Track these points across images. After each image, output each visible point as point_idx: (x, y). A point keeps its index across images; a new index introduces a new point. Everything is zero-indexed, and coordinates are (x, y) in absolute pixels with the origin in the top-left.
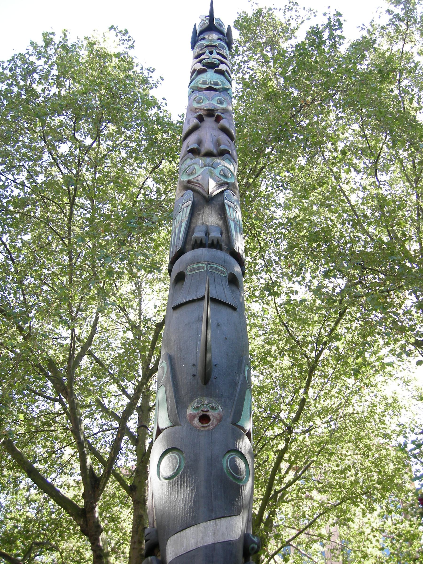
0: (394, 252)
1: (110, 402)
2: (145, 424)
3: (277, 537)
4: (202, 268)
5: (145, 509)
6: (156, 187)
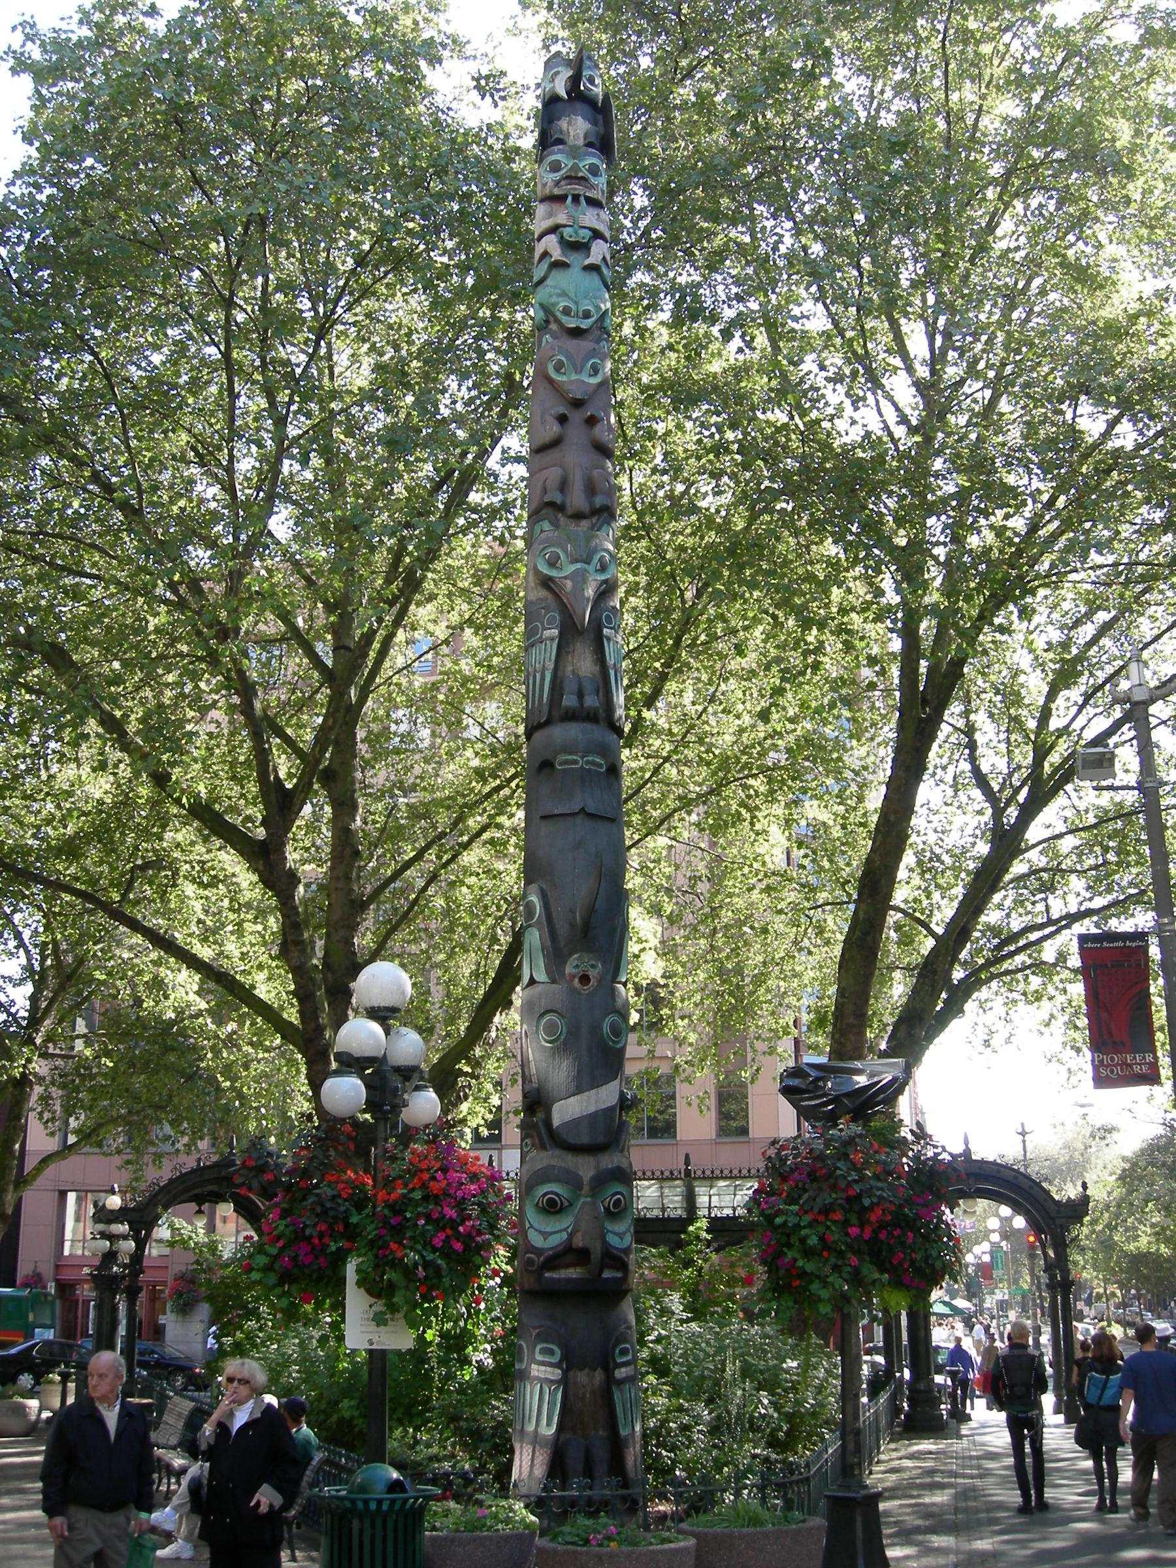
4: (576, 762)
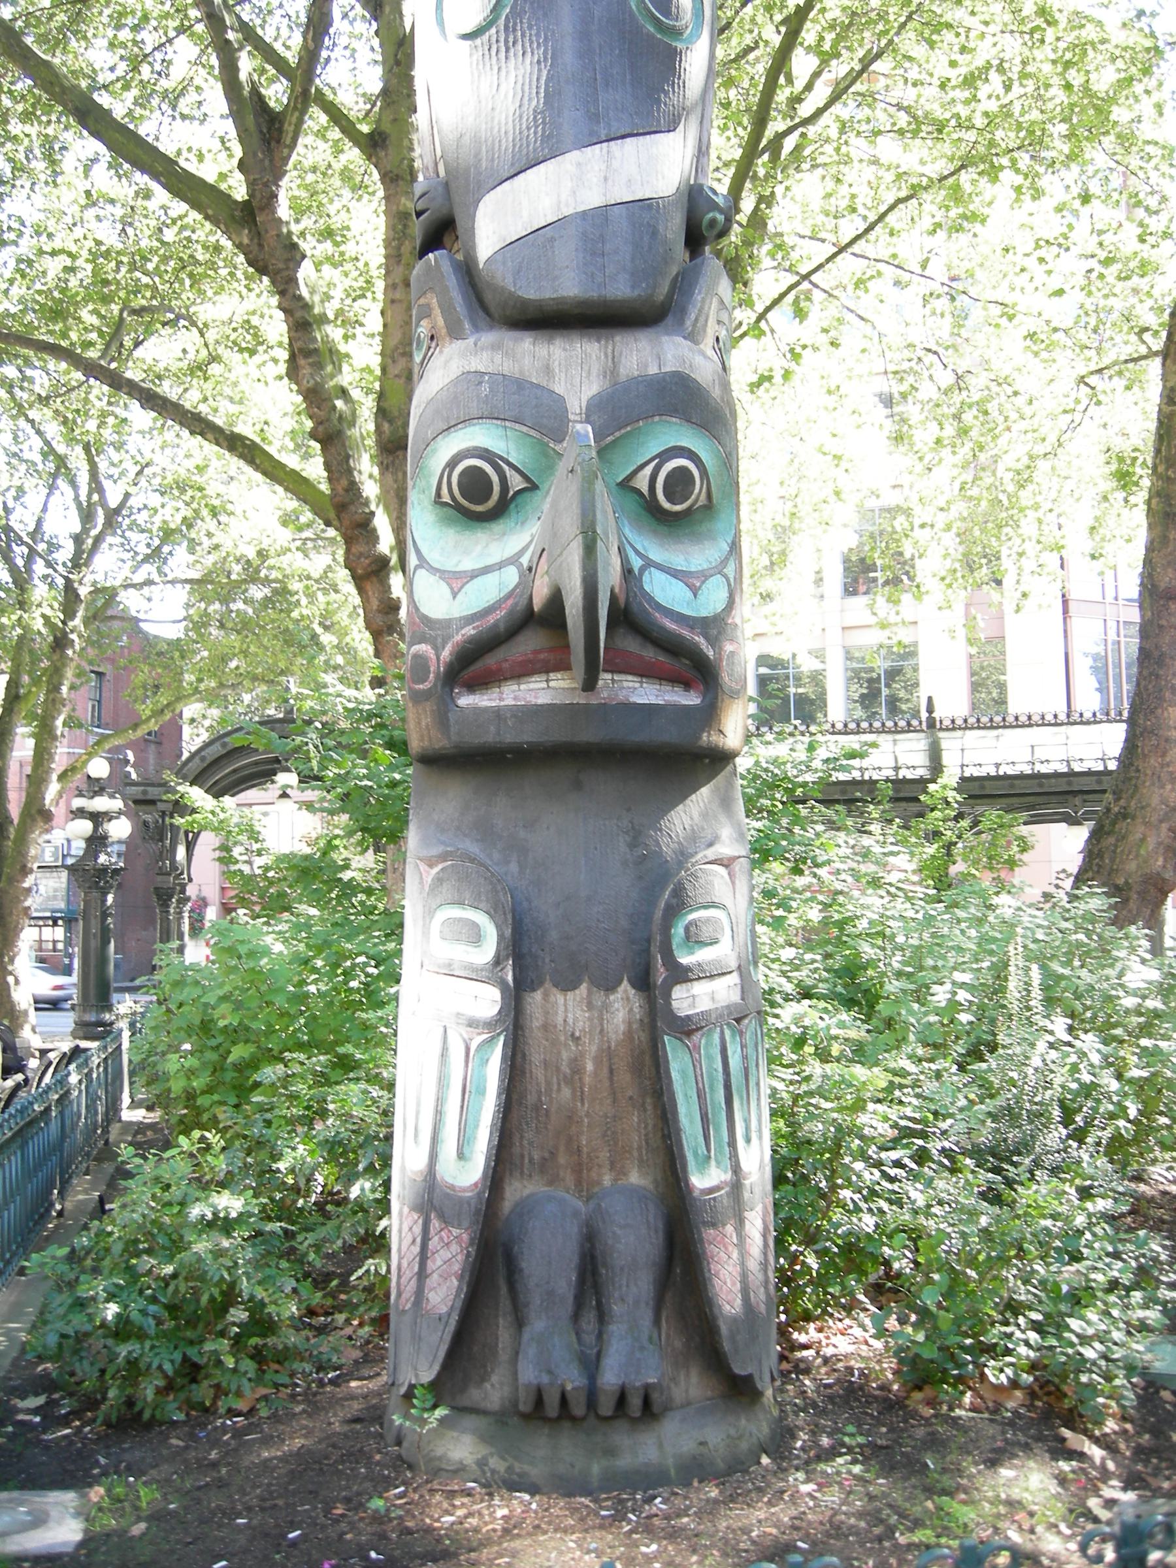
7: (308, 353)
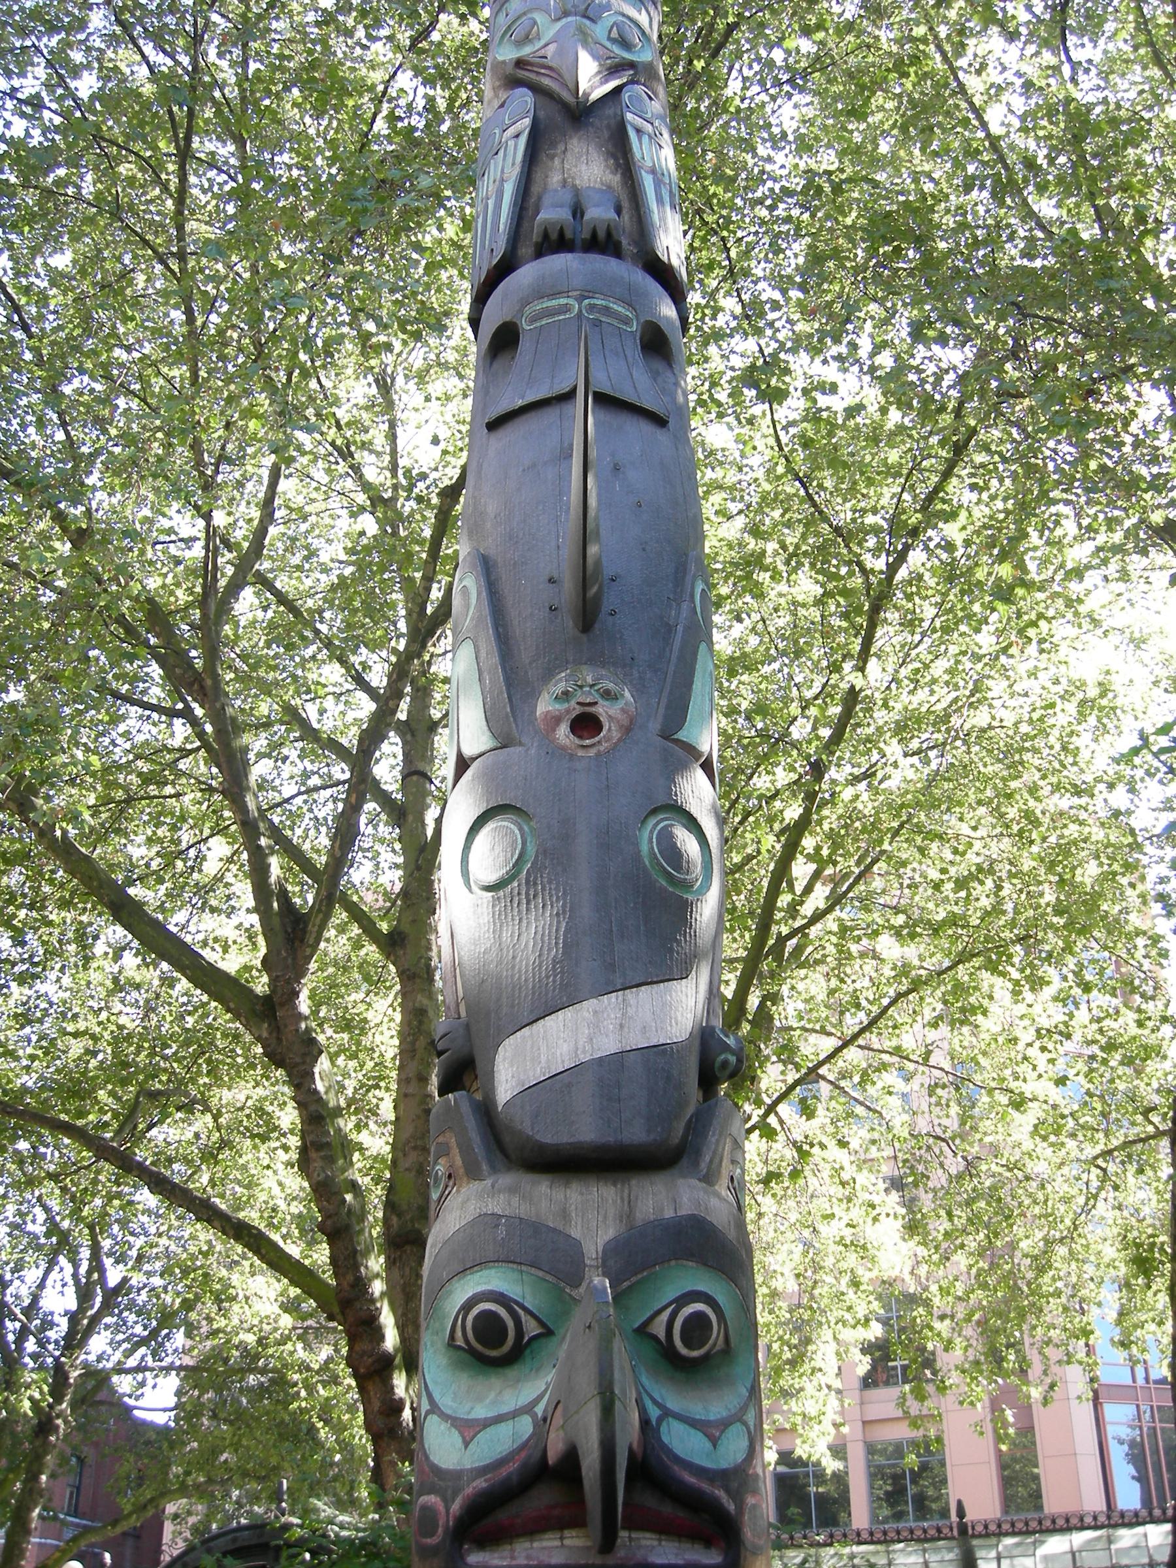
0: (1111, 268)
1: (322, 712)
2: (421, 766)
3: (788, 1053)
4: (566, 309)
5: (431, 995)
6: (426, 96)
7: (320, 1146)
